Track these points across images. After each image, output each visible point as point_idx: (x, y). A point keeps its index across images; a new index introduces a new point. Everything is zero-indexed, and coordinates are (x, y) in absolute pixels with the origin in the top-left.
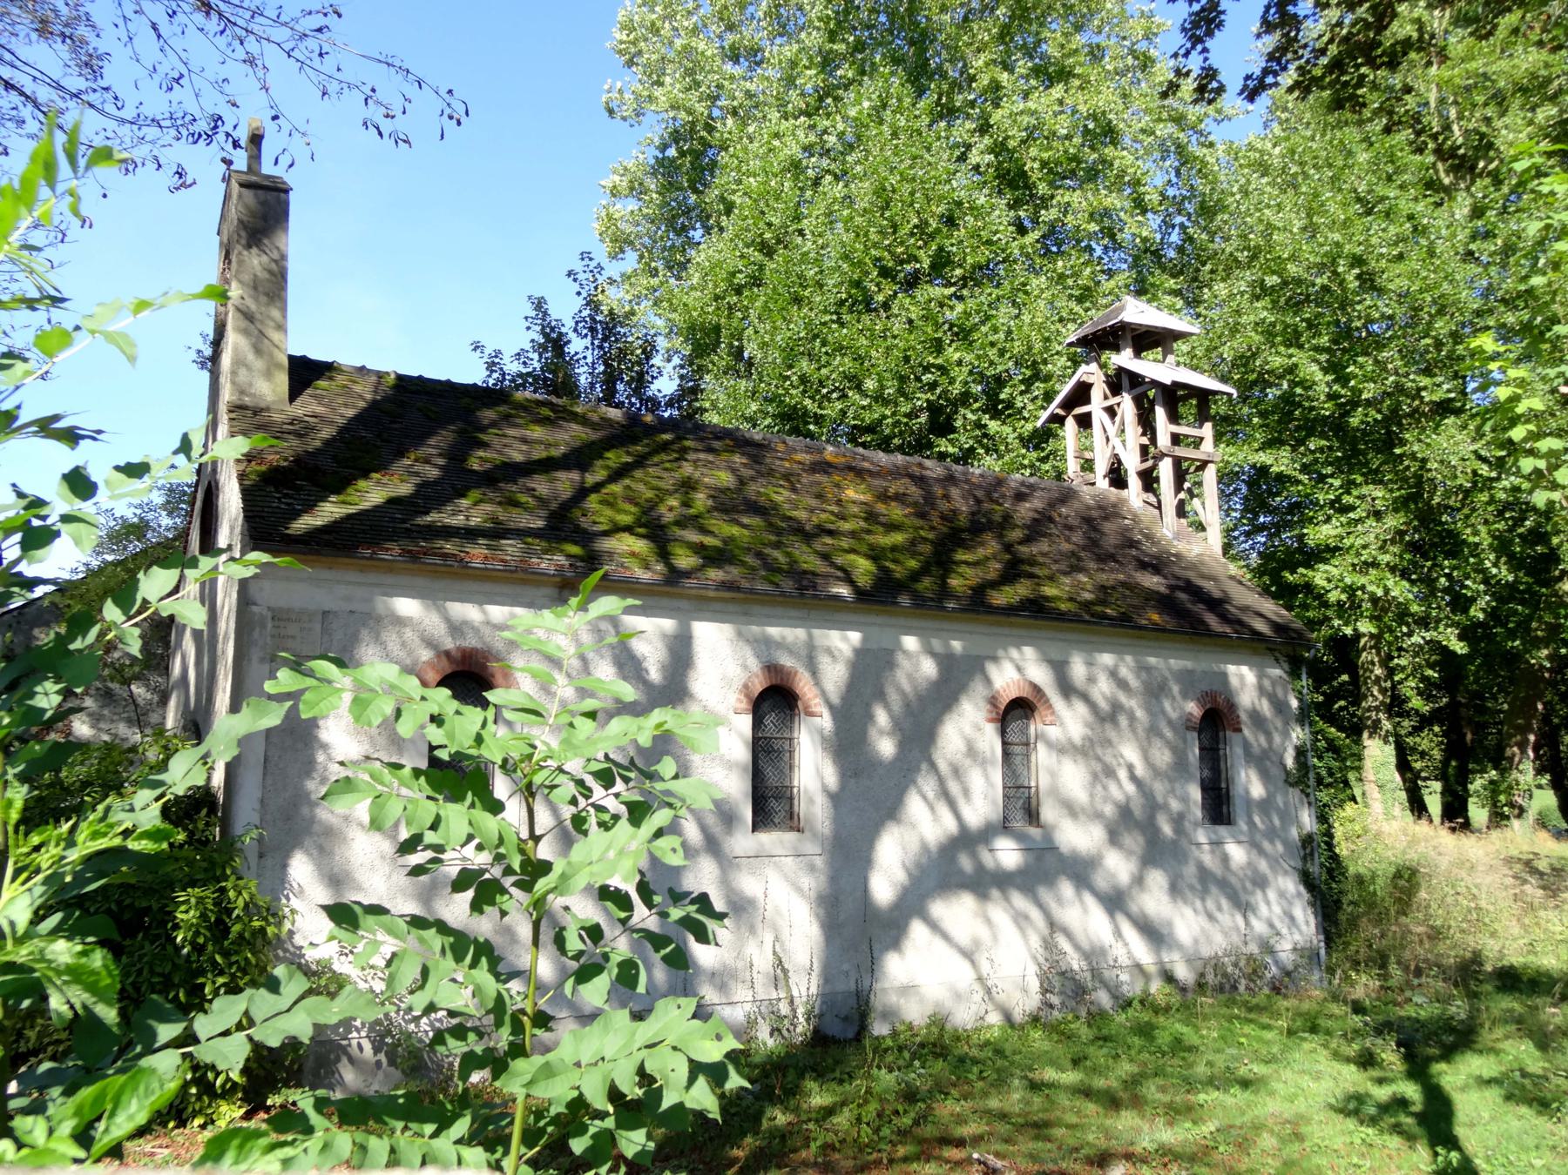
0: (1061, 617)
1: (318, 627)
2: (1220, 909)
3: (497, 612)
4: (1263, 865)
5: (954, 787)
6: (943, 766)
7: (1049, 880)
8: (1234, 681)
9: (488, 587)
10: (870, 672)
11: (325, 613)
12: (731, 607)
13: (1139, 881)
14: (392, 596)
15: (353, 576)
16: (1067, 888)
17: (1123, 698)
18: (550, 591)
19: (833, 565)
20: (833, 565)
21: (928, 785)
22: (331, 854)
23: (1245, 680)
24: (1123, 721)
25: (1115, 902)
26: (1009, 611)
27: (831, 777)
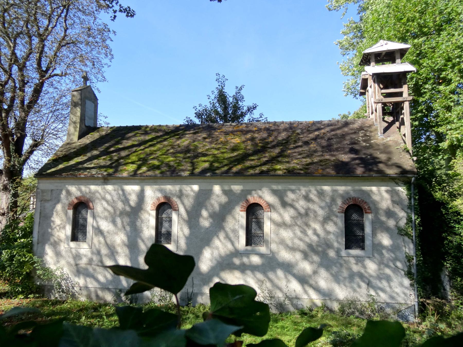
0: (298, 175)
1: (50, 193)
2: (359, 286)
3: (93, 187)
4: (382, 272)
5: (231, 235)
6: (227, 229)
7: (273, 269)
8: (376, 198)
9: (87, 181)
10: (202, 199)
11: (52, 190)
12: (151, 181)
13: (315, 272)
14: (91, 185)
15: (58, 181)
16: (280, 273)
17: (311, 206)
18: (102, 181)
19: (144, 176)
20: (144, 176)
21: (222, 235)
22: (56, 248)
23: (380, 194)
24: (312, 215)
25: (303, 280)
26: (252, 175)
27: (187, 231)
